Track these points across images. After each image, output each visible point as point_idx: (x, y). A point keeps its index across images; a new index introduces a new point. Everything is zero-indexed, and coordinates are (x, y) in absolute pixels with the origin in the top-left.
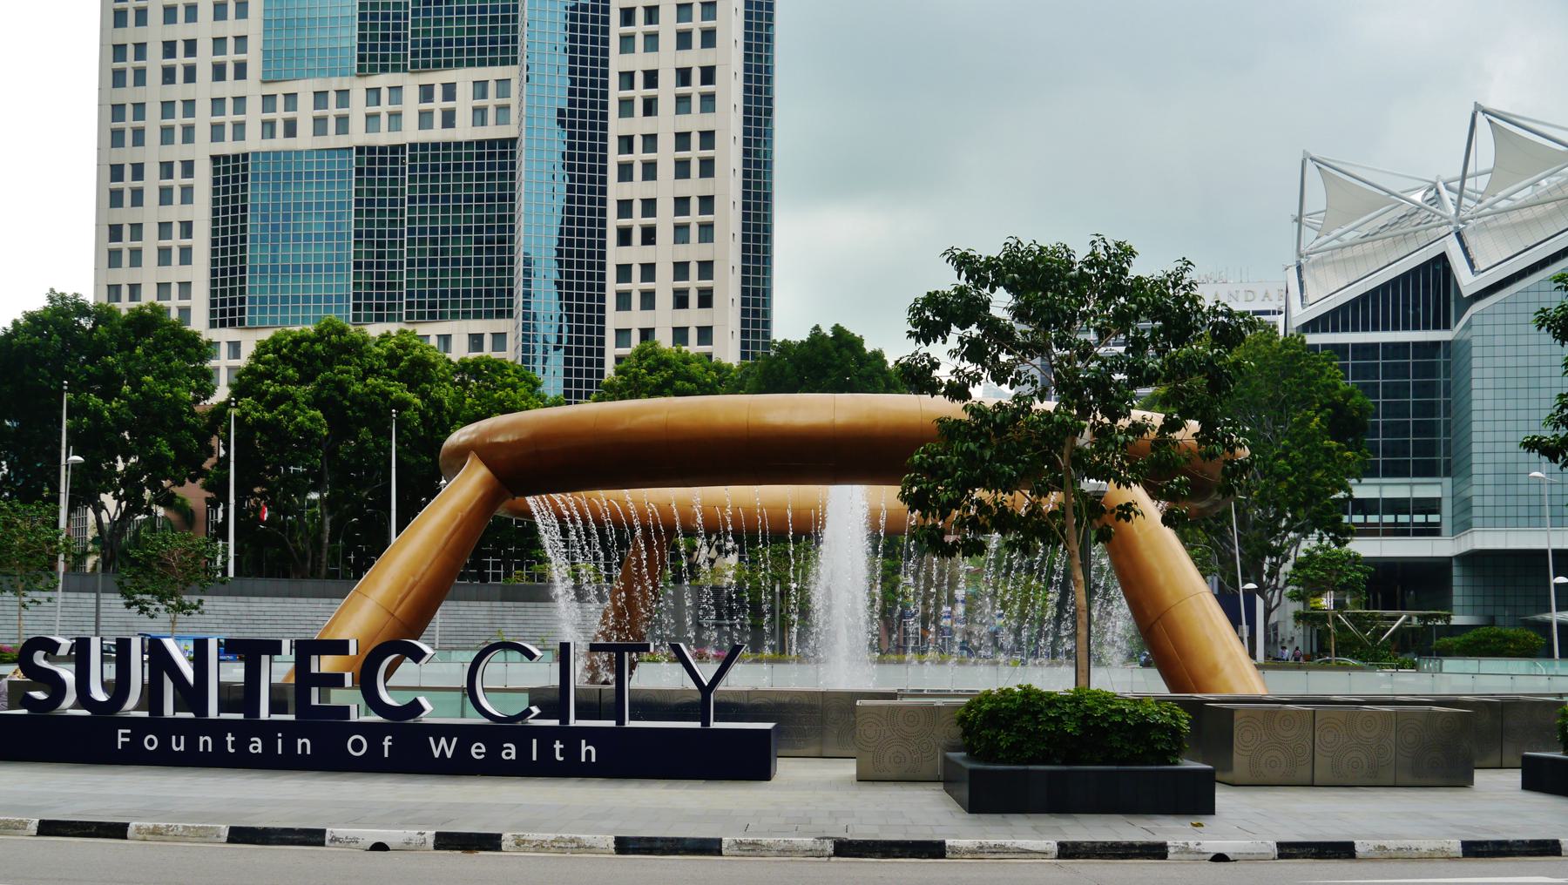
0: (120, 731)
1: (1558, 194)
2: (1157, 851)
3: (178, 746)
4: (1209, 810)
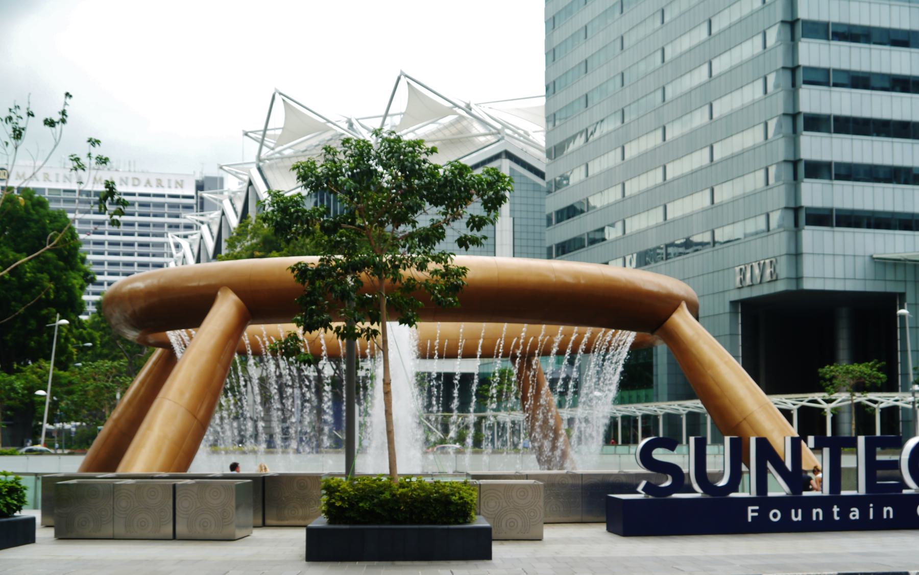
0: (750, 508)
1: (440, 136)
3: (775, 516)
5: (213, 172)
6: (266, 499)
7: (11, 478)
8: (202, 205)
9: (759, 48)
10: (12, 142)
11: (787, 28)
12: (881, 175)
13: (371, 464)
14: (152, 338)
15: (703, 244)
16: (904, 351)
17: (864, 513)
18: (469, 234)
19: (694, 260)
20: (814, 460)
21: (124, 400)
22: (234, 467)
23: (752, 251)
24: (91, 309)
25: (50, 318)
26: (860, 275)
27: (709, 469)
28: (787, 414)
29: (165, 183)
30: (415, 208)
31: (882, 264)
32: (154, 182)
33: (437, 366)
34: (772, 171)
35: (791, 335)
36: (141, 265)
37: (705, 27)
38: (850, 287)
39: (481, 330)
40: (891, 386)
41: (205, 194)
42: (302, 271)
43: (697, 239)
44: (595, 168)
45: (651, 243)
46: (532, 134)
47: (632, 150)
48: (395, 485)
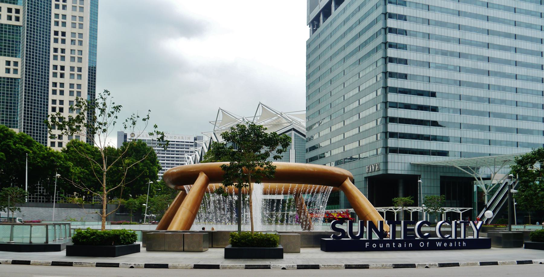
1: (272, 123)
2: (267, 267)
3: (381, 246)
4: (282, 258)
5: (200, 135)
6: (212, 239)
7: (132, 232)
8: (196, 145)
9: (375, 96)
10: (132, 126)
11: (384, 89)
12: (414, 137)
13: (246, 228)
14: (179, 188)
15: (356, 159)
16: (420, 193)
17: (403, 245)
18: (277, 155)
19: (353, 164)
20: (387, 228)
21: (170, 207)
22: (203, 229)
23: (371, 161)
24: (161, 178)
25: (147, 181)
26: (406, 169)
27: (353, 231)
28: (382, 214)
29: (184, 138)
30: (260, 148)
31: (413, 165)
32: (181, 138)
33: (269, 197)
34: (379, 135)
35: (383, 188)
36: (176, 164)
37: (358, 89)
38: (403, 173)
39: (283, 186)
40: (416, 205)
41: (197, 142)
42: (224, 167)
43: (354, 157)
44: (322, 134)
45: (339, 158)
46: (302, 124)
47: (334, 128)
48: (253, 235)
